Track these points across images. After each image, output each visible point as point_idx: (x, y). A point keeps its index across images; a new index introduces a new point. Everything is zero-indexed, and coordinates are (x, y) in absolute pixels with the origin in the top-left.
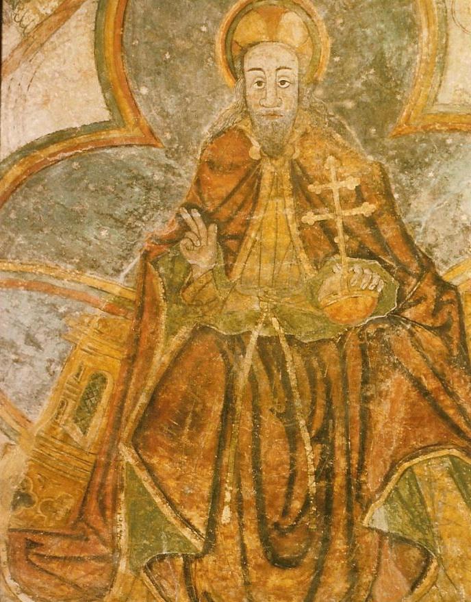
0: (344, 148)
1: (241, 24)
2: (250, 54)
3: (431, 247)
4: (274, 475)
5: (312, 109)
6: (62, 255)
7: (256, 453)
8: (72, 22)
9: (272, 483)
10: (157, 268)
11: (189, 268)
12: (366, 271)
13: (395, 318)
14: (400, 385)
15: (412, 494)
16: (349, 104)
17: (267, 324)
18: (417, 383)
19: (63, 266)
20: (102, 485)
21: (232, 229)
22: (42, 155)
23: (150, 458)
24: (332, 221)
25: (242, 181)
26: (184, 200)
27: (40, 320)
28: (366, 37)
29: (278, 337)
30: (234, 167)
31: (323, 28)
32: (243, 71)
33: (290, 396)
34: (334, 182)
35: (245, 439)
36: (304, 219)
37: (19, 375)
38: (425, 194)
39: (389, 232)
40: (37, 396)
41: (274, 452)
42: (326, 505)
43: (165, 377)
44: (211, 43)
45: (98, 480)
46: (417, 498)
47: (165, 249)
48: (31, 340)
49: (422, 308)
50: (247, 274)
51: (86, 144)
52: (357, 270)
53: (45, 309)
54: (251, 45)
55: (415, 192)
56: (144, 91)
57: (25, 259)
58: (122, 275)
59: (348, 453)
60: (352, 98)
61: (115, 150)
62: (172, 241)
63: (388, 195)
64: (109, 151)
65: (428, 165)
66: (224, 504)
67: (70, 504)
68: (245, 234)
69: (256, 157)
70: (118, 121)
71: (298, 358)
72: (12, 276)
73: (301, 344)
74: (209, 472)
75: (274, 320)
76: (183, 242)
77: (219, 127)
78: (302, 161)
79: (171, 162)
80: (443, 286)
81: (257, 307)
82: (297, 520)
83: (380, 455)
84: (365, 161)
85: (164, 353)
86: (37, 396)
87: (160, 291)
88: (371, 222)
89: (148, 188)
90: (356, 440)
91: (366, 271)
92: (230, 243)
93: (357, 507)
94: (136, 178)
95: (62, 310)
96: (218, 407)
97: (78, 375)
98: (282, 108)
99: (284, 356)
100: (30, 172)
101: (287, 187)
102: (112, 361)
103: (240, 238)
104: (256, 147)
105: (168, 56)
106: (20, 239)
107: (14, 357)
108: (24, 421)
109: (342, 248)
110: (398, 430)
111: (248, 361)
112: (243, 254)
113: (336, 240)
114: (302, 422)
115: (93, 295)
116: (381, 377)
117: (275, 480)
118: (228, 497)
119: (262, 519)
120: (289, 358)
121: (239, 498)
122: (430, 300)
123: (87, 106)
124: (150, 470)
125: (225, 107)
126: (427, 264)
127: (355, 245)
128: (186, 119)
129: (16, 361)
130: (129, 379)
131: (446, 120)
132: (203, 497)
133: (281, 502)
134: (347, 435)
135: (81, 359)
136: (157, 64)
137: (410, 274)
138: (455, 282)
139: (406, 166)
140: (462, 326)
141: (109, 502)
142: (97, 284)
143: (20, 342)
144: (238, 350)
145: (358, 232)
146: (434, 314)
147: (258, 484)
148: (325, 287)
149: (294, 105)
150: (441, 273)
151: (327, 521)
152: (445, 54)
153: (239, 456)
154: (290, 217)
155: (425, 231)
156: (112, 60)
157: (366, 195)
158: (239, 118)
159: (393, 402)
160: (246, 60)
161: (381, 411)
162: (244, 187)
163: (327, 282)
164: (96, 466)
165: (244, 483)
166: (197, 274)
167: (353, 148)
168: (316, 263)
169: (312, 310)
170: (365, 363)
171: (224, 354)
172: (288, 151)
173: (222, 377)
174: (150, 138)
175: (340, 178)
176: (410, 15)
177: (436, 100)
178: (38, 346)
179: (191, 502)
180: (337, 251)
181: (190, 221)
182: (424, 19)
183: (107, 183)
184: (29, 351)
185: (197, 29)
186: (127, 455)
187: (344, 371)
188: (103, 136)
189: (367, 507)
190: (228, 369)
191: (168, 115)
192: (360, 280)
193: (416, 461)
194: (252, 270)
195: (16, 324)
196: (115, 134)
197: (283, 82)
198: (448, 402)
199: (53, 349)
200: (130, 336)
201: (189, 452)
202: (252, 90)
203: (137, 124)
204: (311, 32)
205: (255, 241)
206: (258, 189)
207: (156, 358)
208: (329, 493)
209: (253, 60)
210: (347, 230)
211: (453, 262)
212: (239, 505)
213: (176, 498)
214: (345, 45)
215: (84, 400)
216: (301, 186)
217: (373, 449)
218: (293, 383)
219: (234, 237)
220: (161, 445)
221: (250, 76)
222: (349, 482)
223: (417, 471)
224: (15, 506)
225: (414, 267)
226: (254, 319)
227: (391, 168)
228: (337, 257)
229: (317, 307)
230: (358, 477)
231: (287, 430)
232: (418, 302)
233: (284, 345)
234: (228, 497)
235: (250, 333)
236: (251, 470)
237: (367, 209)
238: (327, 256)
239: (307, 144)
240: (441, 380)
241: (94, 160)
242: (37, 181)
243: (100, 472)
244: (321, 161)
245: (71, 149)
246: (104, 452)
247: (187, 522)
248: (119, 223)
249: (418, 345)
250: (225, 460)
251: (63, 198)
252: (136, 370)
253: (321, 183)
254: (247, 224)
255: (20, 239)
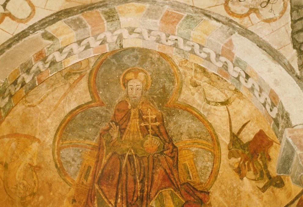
0: (153, 107)
1: (127, 75)
2: (129, 82)
3: (172, 136)
4: (130, 191)
5: (145, 97)
6: (80, 136)
7: (126, 185)
8: (83, 80)
9: (130, 193)
10: (103, 137)
11: (112, 137)
12: (156, 140)
13: (162, 153)
14: (161, 171)
15: (161, 198)
16: (155, 97)
17: (130, 151)
18: (165, 170)
19: (80, 140)
20: (91, 195)
21: (123, 127)
22: (74, 112)
23: (102, 187)
24: (148, 126)
25: (125, 115)
26: (111, 120)
27: (76, 154)
28: (161, 81)
29: (133, 155)
30: (124, 111)
31: (150, 78)
32: (127, 86)
33: (135, 170)
34: (150, 116)
35: (124, 181)
36: (141, 124)
37: (71, 169)
38: (172, 123)
39: (162, 130)
40: (75, 174)
41: (131, 185)
42: (142, 200)
43: (105, 165)
44: (119, 80)
45: (90, 193)
46: (162, 200)
47: (106, 132)
48: (73, 160)
49: (168, 151)
50: (126, 138)
51: (86, 107)
52: (154, 139)
53: (77, 151)
54: (130, 80)
55: (170, 122)
56: (101, 92)
57: (71, 139)
58: (95, 140)
59: (148, 187)
60: (156, 95)
61: (93, 108)
62: (107, 130)
63: (163, 121)
64: (91, 108)
65: (174, 116)
66: (119, 198)
67: (84, 200)
68: (126, 128)
69: (130, 108)
70: (94, 100)
71: (137, 161)
72: (68, 144)
73: (138, 157)
74: (116, 190)
75: (132, 150)
76: (110, 130)
77: (120, 100)
78: (141, 109)
79: (108, 110)
80: (174, 147)
81: (128, 147)
82: (135, 202)
83: (155, 188)
84: (158, 111)
85: (105, 159)
86: (75, 174)
87: (104, 143)
88: (158, 127)
89: (101, 117)
90: (150, 183)
91: (156, 140)
92: (122, 131)
93: (149, 201)
94: (98, 115)
95: (80, 151)
96: (118, 173)
97: (85, 167)
98: (137, 96)
99: (134, 160)
100: (72, 117)
101: (137, 116)
102: (92, 162)
103: (125, 129)
104: (130, 105)
105: (107, 83)
106: (70, 134)
107: (70, 165)
108: (73, 181)
109: (150, 133)
110: (160, 182)
111: (125, 161)
112: (125, 133)
113: (149, 131)
114: (137, 177)
115: (88, 146)
116: (157, 168)
117: (131, 191)
118: (120, 196)
119: (127, 202)
120: (135, 160)
121: (122, 196)
122: (171, 149)
123: (88, 98)
124: (102, 190)
125: (123, 94)
126: (171, 141)
127: (154, 132)
128: (112, 99)
129: (70, 166)
130: (97, 167)
131: (180, 105)
132: (114, 196)
133: (131, 198)
134: (148, 182)
135: (85, 162)
136: (104, 85)
137: (166, 142)
138: (177, 146)
139: (168, 115)
140: (177, 158)
141: (93, 199)
142: (89, 143)
143: (71, 161)
144: (123, 158)
145: (155, 129)
146: (171, 153)
147: (127, 192)
148: (145, 143)
149: (141, 95)
150: (174, 143)
151: (142, 203)
152: (181, 90)
153: (122, 186)
154: (138, 124)
155: (171, 132)
156: (92, 86)
157: (157, 120)
158: (126, 98)
159: (159, 175)
160: (128, 83)
161: (156, 177)
162: (126, 116)
163: (146, 141)
164: (89, 190)
165: (123, 192)
166: (114, 139)
167: (155, 108)
168: (143, 136)
169: (141, 148)
170: (154, 164)
171: (119, 159)
172: (138, 107)
173: (119, 165)
174: (102, 104)
175: (151, 115)
176: (173, 79)
177: (177, 100)
178: (75, 161)
179: (111, 198)
180: (149, 134)
181: (112, 125)
182: (176, 81)
183: (91, 116)
184: (73, 163)
185: (135, 202)
186: (97, 187)
187: (148, 165)
188: (90, 105)
189: (151, 200)
190: (121, 163)
191: (107, 98)
192: (154, 142)
193: (163, 190)
194: (127, 137)
195: (70, 156)
196: (93, 104)
197: (138, 89)
198: (172, 176)
199: (78, 161)
200: (97, 155)
201: (111, 185)
202: (130, 91)
203: (99, 101)
204: (146, 78)
205: (128, 130)
206: (130, 116)
207: (103, 161)
208: (143, 196)
209: (130, 83)
210: (152, 128)
211: (177, 141)
212: (122, 198)
213: (108, 197)
214: (155, 82)
215: (86, 173)
216: (141, 118)
217: (154, 186)
218: (136, 167)
219: (123, 129)
220: (104, 183)
221: (129, 87)
222: (147, 194)
223: (163, 193)
224: (72, 203)
225: (168, 140)
226: (127, 150)
227: (164, 114)
228: (149, 135)
229: (143, 147)
230: (150, 193)
231: (134, 179)
232: (168, 149)
233: (134, 157)
234: (120, 196)
235: (126, 154)
236: (125, 189)
237: (157, 124)
238: (146, 134)
239: (143, 105)
240: (171, 171)
241: (87, 111)
242: (74, 119)
243: (91, 191)
244: (146, 110)
245: (82, 109)
246: (45, 30)
247: (110, 203)
248: (94, 126)
249: (167, 160)
250: (119, 187)
251: (80, 122)
252: (98, 164)
253: (146, 116)
254: (127, 126)
255: (70, 134)
